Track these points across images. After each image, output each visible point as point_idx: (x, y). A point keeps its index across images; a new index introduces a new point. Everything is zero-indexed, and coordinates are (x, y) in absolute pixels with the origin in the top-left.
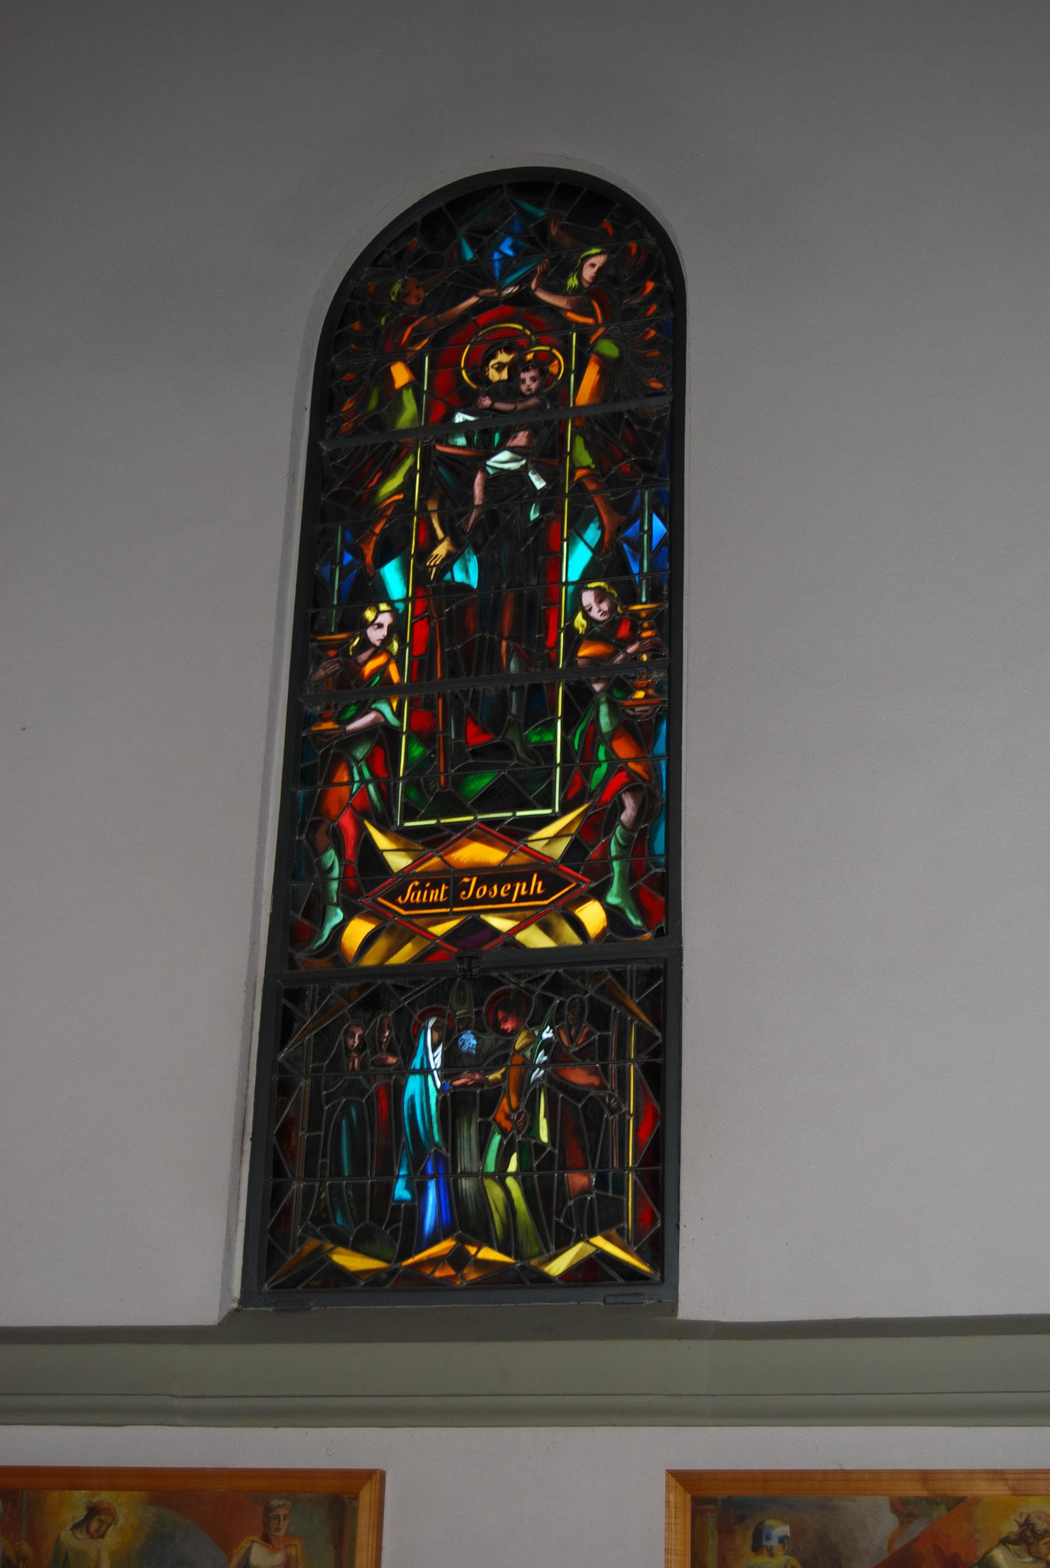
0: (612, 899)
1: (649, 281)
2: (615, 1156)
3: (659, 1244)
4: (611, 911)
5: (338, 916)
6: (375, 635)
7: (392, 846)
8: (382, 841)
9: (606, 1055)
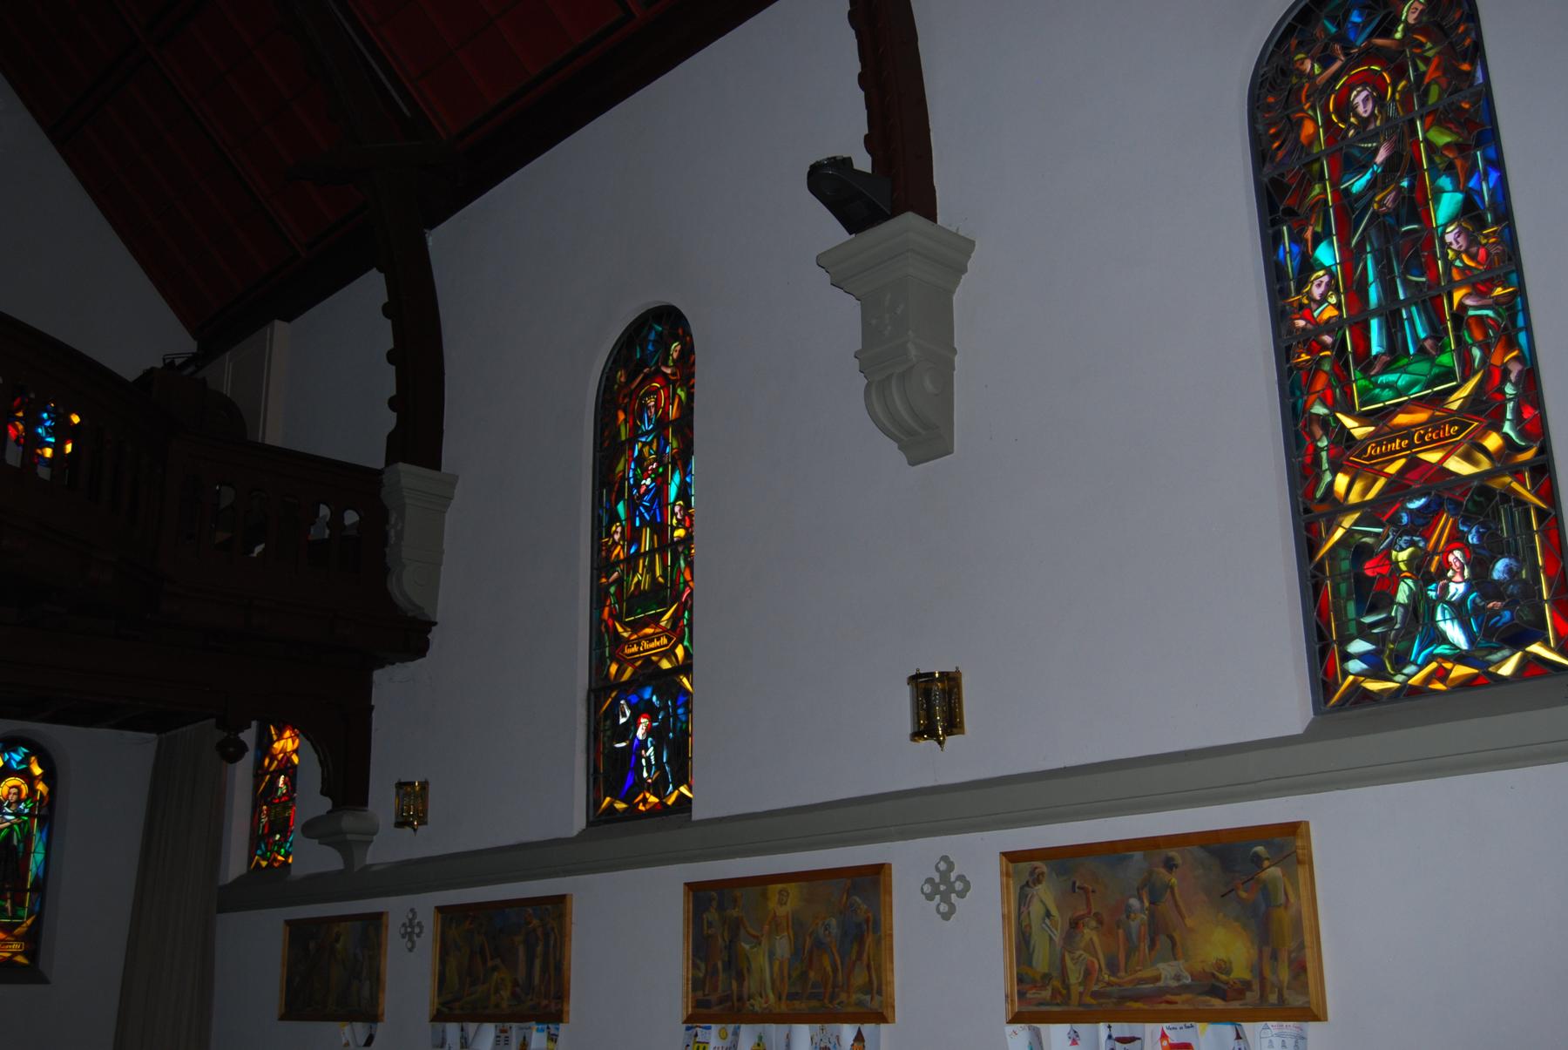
5: (1328, 477)
6: (1317, 292)
8: (1348, 422)
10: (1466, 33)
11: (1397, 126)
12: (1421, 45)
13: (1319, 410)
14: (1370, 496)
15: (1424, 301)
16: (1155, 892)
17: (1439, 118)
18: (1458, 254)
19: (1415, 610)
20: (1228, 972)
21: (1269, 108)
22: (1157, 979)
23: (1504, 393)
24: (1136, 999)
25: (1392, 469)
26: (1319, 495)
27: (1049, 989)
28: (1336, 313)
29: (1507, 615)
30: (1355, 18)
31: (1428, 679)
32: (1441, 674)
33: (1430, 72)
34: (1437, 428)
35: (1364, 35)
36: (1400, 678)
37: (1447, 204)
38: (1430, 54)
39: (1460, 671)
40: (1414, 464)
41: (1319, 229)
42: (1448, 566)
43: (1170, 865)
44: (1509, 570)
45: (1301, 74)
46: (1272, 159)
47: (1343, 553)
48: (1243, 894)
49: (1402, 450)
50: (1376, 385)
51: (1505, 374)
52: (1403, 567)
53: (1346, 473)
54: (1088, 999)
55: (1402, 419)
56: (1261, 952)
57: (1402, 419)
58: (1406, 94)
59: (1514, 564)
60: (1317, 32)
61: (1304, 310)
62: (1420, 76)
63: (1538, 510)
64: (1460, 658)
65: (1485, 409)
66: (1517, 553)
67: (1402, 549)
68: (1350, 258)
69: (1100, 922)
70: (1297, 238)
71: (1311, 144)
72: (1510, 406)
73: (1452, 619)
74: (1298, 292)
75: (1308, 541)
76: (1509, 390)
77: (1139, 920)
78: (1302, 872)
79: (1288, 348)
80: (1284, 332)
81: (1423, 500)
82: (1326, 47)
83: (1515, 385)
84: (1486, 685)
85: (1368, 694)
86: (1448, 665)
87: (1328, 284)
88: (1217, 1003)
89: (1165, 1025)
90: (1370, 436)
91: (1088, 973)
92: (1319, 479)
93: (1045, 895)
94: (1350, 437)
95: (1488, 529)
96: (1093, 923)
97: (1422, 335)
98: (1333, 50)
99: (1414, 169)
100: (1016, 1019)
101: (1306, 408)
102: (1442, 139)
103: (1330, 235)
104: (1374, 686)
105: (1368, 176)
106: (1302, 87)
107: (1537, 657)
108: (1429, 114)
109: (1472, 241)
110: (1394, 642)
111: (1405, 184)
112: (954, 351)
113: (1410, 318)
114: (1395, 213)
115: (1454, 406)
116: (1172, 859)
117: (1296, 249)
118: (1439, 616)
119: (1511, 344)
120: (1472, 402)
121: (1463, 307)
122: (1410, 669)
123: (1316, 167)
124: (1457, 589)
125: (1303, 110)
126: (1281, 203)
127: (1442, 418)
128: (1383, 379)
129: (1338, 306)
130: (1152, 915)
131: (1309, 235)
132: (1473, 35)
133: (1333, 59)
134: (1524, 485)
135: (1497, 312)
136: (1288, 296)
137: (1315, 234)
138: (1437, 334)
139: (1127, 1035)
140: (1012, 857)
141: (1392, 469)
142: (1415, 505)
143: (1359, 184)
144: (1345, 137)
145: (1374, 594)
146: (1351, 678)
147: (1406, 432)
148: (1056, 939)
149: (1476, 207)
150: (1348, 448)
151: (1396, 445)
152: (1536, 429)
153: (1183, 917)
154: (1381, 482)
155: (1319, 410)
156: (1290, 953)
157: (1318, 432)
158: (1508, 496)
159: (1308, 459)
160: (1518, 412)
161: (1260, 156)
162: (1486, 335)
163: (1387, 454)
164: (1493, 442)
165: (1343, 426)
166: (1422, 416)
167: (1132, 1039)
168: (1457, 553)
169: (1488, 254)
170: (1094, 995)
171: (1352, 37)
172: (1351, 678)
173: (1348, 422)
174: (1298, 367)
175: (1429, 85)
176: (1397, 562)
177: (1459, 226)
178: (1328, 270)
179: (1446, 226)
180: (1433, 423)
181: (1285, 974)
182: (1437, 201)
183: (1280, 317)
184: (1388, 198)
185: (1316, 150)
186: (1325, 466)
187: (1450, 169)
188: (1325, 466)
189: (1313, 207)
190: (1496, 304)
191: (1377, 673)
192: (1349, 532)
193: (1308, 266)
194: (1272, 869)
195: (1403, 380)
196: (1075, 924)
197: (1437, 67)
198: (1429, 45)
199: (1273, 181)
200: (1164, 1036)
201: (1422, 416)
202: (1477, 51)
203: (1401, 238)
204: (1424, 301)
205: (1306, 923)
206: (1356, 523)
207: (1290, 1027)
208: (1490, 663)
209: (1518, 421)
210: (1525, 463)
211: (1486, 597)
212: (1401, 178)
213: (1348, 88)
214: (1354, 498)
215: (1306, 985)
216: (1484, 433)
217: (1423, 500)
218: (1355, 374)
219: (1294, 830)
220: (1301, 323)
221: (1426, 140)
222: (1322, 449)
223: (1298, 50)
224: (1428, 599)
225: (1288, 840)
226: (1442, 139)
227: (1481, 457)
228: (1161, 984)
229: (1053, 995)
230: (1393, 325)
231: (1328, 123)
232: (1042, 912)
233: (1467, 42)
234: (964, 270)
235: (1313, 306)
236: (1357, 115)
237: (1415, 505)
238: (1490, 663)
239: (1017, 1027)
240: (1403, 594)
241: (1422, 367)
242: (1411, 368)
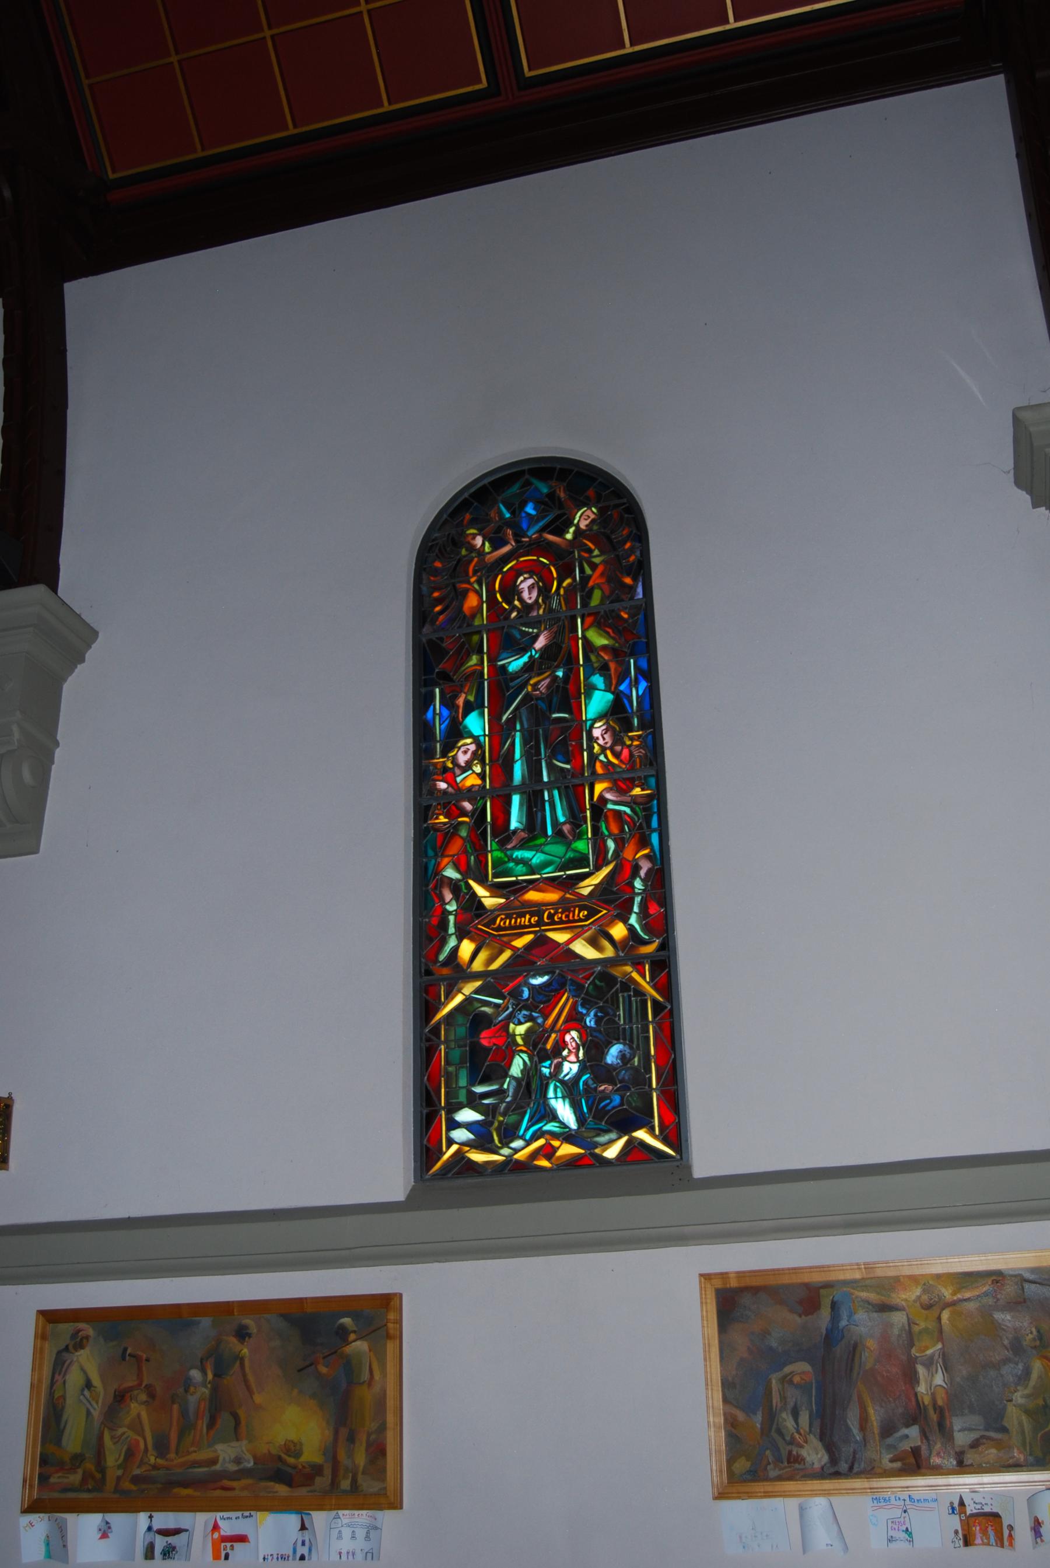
0: (633, 920)
1: (623, 519)
2: (642, 1087)
3: (675, 1134)
4: (631, 929)
5: (452, 942)
6: (462, 759)
7: (488, 894)
8: (480, 891)
9: (633, 1018)
10: (632, 550)
11: (559, 619)
12: (590, 551)
13: (451, 873)
14: (495, 966)
15: (567, 787)
16: (220, 1363)
17: (601, 621)
18: (603, 749)
19: (528, 1085)
20: (298, 1454)
21: (436, 572)
22: (214, 1461)
23: (633, 887)
24: (185, 1485)
25: (520, 943)
26: (442, 957)
27: (80, 1471)
28: (479, 782)
29: (617, 1099)
30: (530, 509)
31: (534, 1155)
32: (548, 1152)
33: (596, 578)
34: (566, 910)
35: (537, 527)
36: (506, 1151)
37: (598, 702)
38: (597, 560)
39: (567, 1150)
40: (542, 942)
41: (471, 698)
42: (565, 1045)
43: (242, 1334)
44: (622, 1056)
45: (471, 548)
46: (433, 622)
47: (460, 1019)
48: (323, 1370)
49: (531, 926)
50: (511, 859)
51: (636, 868)
52: (519, 1040)
53: (472, 940)
54: (127, 1485)
55: (532, 896)
56: (336, 1433)
57: (532, 896)
58: (571, 591)
59: (628, 1050)
60: (492, 514)
61: (446, 773)
62: (585, 579)
63: (655, 1002)
64: (568, 1137)
65: (614, 898)
66: (631, 1041)
67: (520, 1023)
68: (499, 732)
69: (152, 1395)
70: (448, 702)
71: (473, 616)
72: (638, 900)
73: (563, 1098)
74: (444, 754)
75: (425, 1004)
76: (638, 884)
77: (199, 1394)
78: (390, 1346)
79: (428, 808)
80: (424, 791)
81: (546, 978)
82: (499, 530)
83: (644, 881)
84: (591, 1165)
85: (472, 1165)
86: (556, 1143)
87: (474, 753)
88: (282, 1490)
89: (219, 1515)
90: (500, 908)
91: (130, 1454)
92: (444, 941)
93: (87, 1362)
94: (481, 905)
95: (606, 1014)
96: (143, 1397)
97: (562, 819)
98: (505, 534)
99: (571, 661)
100: (33, 1507)
101: (438, 871)
102: (600, 640)
103: (483, 706)
104: (478, 1157)
105: (525, 659)
106: (472, 561)
107: (643, 1144)
108: (590, 615)
109: (617, 740)
110: (504, 1114)
111: (560, 674)
112: (57, 744)
113: (551, 796)
114: (548, 698)
115: (585, 892)
116: (246, 1327)
117: (446, 713)
118: (551, 1094)
119: (644, 842)
120: (603, 891)
121: (603, 800)
122: (517, 1144)
123: (476, 638)
124: (570, 1068)
125: (469, 582)
126: (437, 664)
127: (573, 901)
128: (519, 854)
129: (482, 776)
130: (215, 1389)
131: (461, 701)
132: (638, 553)
133: (505, 543)
134: (644, 977)
135: (632, 810)
136: (433, 757)
137: (467, 703)
138: (576, 819)
139: (172, 1525)
140: (50, 1317)
141: (520, 943)
142: (538, 981)
143: (516, 664)
144: (507, 618)
145: (487, 1064)
146: (454, 1148)
147: (536, 909)
148: (96, 1413)
149: (625, 710)
150: (478, 916)
151: (525, 920)
152: (661, 924)
153: (251, 1392)
154: (507, 954)
155: (451, 873)
156: (369, 1435)
157: (448, 896)
158: (628, 985)
159: (435, 921)
160: (643, 906)
161: (421, 616)
162: (622, 830)
163: (515, 927)
164: (618, 931)
165: (474, 894)
166: (553, 896)
167: (177, 1532)
168: (574, 1034)
169: (631, 755)
170: (136, 1480)
171: (524, 526)
172: (454, 1148)
173: (480, 891)
174: (435, 828)
175: (592, 589)
176: (514, 1035)
177: (607, 723)
178: (476, 740)
179: (595, 721)
180: (564, 905)
181: (361, 1458)
182: (589, 696)
183: (423, 776)
184: (541, 684)
185: (477, 622)
186: (452, 930)
187: (604, 669)
188: (452, 930)
189: (469, 677)
190: (633, 803)
191: (483, 1143)
192: (468, 1000)
193: (456, 732)
194: (358, 1343)
195: (537, 858)
196: (121, 1397)
197: (602, 574)
198: (596, 552)
199: (430, 642)
200: (216, 1527)
201: (553, 896)
202: (642, 569)
203: (552, 725)
204: (567, 787)
205: (390, 1403)
206: (477, 991)
207: (362, 1517)
208: (596, 1145)
209: (644, 914)
210: (646, 956)
211: (598, 1079)
212: (558, 667)
213: (516, 572)
214: (478, 966)
215: (384, 1470)
216: (611, 923)
217: (546, 978)
218: (491, 844)
219: (388, 1302)
220: (443, 785)
221: (584, 637)
222: (450, 913)
223: (472, 523)
224: (542, 1076)
225: (378, 1315)
226: (600, 640)
227: (606, 944)
228: (218, 1467)
229: (84, 1480)
230: (534, 804)
231: (492, 601)
232: (82, 1381)
233: (632, 558)
234: (82, 660)
235: (457, 771)
236: (521, 600)
237: (538, 981)
238: (596, 1145)
239: (34, 1517)
240: (516, 1068)
241: (558, 849)
242: (547, 848)
